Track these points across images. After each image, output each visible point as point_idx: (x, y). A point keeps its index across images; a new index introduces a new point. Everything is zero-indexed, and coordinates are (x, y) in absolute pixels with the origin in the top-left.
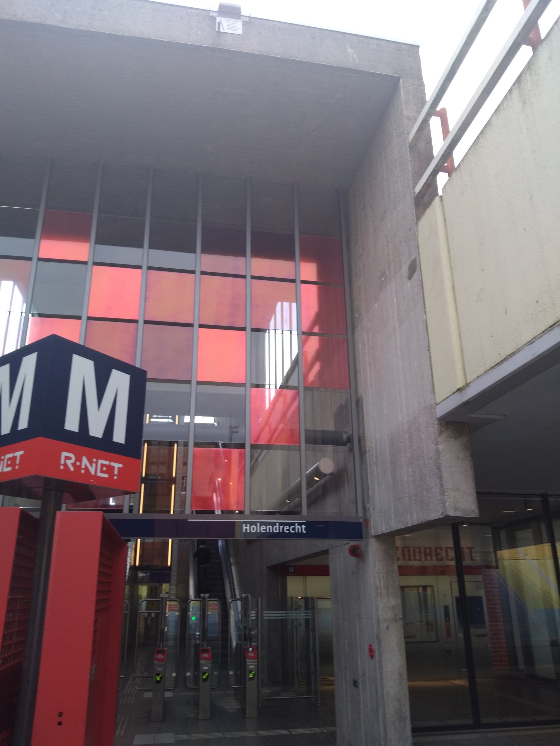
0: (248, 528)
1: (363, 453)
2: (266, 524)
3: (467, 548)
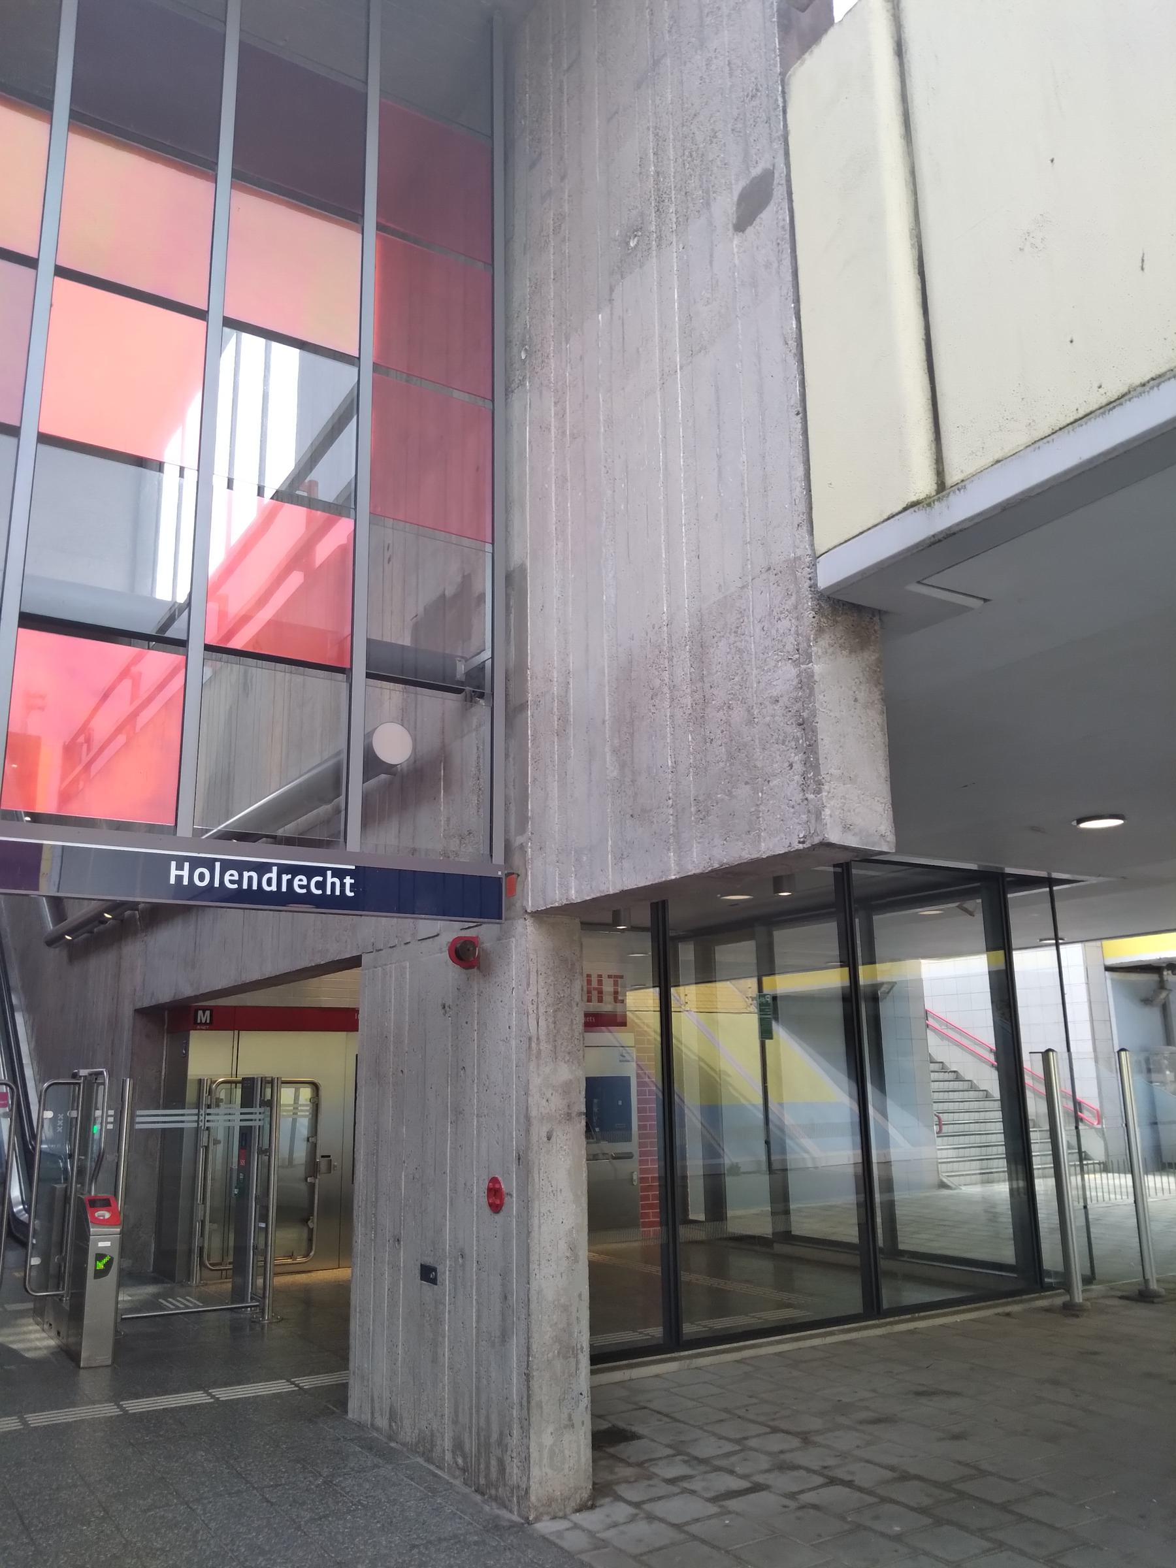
0: (185, 873)
1: (515, 711)
2: (241, 867)
3: (610, 977)
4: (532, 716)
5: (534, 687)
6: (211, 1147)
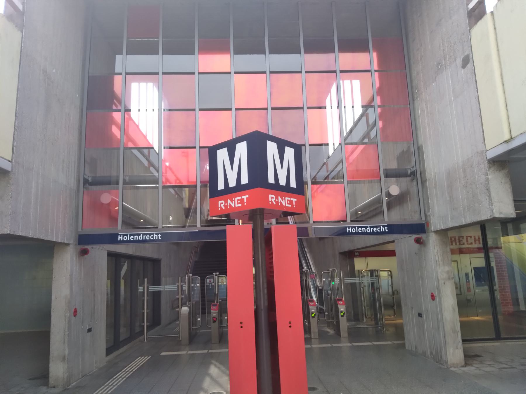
0: (350, 230)
1: (424, 182)
2: (362, 227)
4: (428, 183)
5: (428, 176)
6: (364, 287)
